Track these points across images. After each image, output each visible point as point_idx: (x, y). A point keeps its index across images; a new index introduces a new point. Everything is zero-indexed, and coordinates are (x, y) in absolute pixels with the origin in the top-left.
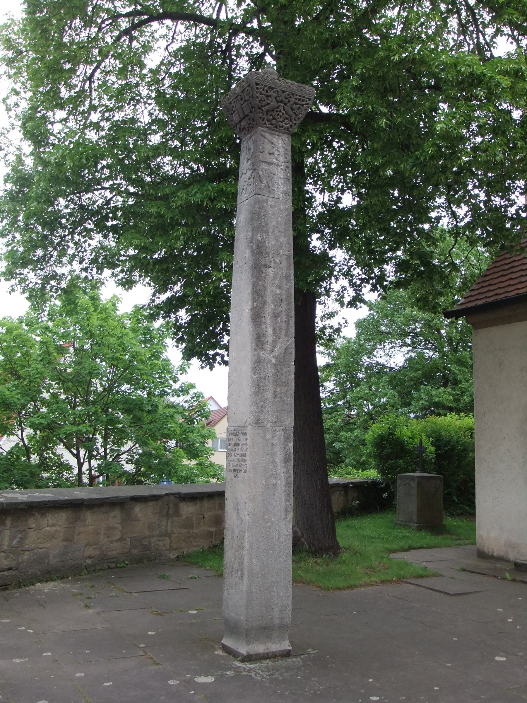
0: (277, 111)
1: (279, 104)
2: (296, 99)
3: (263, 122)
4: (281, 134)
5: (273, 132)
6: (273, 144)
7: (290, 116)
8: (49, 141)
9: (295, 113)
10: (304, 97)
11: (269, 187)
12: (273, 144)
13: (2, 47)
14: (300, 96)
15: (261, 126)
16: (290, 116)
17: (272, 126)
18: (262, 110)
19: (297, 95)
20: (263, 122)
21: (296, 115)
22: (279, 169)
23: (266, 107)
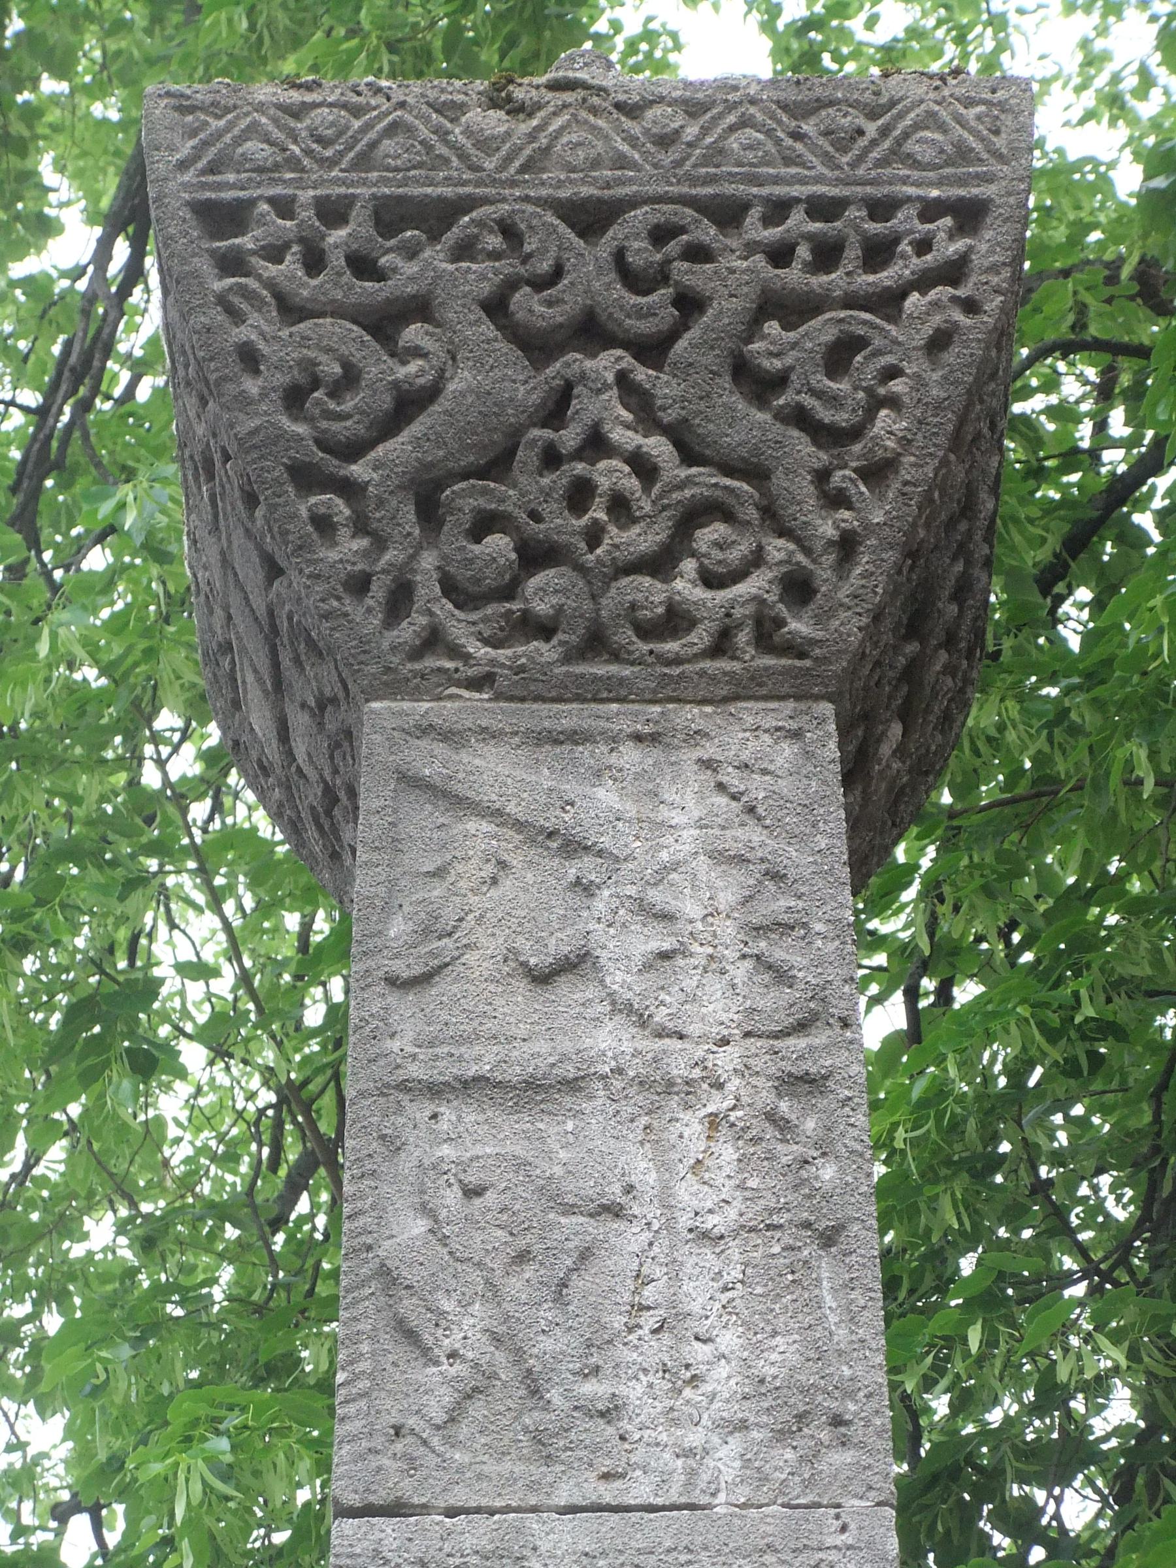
0: (552, 458)
1: (575, 362)
2: (780, 255)
3: (408, 631)
4: (690, 715)
5: (570, 716)
6: (573, 847)
7: (756, 473)
8: (178, 1155)
9: (800, 418)
10: (881, 209)
11: (533, 1386)
12: (573, 847)
13: (1169, 266)
14: (823, 209)
15: (394, 687)
16: (756, 473)
17: (545, 651)
18: (349, 489)
19: (778, 210)
20: (408, 631)
21: (822, 434)
22: (691, 1126)
23: (397, 448)
